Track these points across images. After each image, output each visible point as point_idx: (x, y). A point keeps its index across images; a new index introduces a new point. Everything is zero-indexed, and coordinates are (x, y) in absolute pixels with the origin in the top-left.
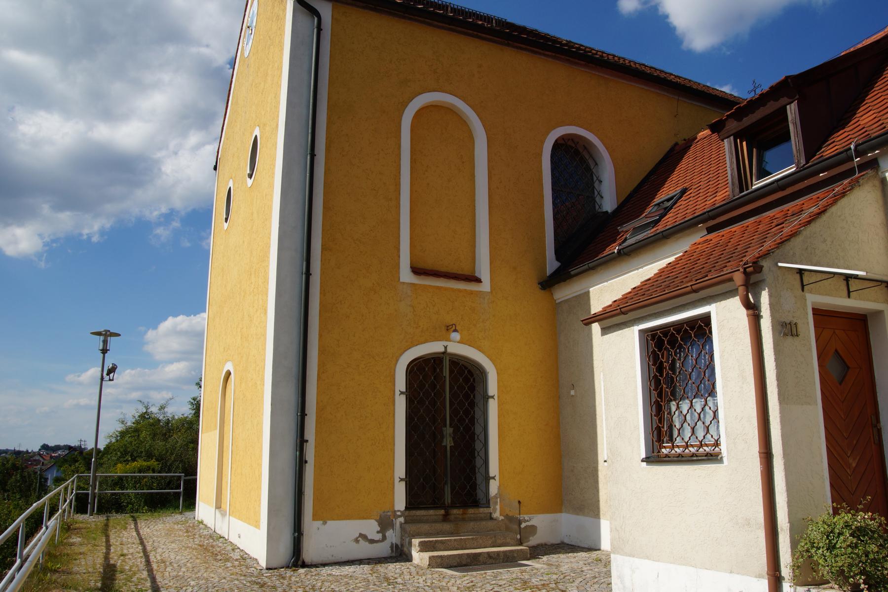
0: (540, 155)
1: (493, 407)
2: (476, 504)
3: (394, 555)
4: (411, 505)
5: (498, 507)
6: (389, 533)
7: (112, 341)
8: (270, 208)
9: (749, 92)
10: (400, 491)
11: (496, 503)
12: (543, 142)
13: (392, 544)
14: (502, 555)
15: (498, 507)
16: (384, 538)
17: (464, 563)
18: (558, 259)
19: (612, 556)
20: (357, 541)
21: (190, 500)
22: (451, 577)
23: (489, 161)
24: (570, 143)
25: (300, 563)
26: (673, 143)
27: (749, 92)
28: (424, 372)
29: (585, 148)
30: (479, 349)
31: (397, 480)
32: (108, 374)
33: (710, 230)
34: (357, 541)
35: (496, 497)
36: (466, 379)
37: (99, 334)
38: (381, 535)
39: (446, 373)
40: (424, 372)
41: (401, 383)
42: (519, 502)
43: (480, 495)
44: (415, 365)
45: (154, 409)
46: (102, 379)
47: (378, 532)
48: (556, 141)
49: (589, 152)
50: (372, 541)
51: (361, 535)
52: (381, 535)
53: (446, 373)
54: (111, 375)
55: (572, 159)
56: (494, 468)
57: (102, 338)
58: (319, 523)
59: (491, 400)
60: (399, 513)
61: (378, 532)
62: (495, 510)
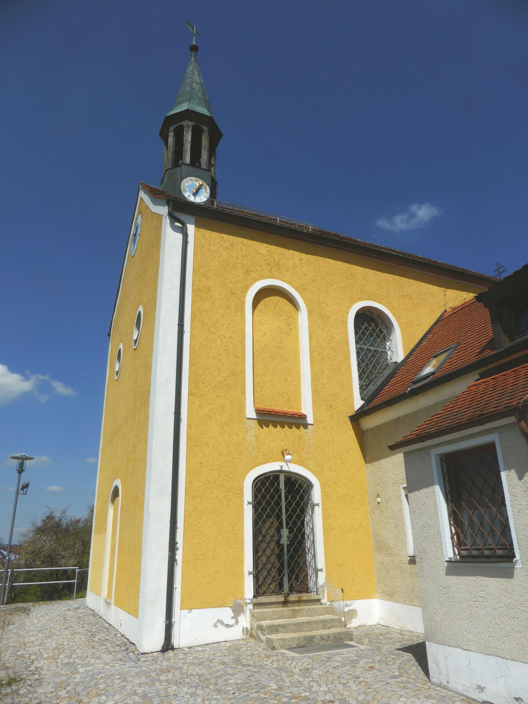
0: (345, 322)
1: (318, 512)
2: (307, 590)
3: (244, 637)
4: (257, 593)
5: (326, 594)
6: (241, 618)
7: (27, 463)
8: (242, 542)
9: (494, 271)
10: (249, 583)
11: (323, 590)
12: (347, 313)
13: (244, 628)
14: (331, 636)
15: (326, 594)
16: (237, 622)
17: (302, 644)
18: (362, 399)
19: (427, 643)
20: (215, 626)
21: (82, 588)
22: (293, 659)
23: (310, 327)
24: (368, 313)
25: (170, 647)
26: (443, 310)
27: (494, 271)
28: (269, 490)
29: (379, 316)
30: (307, 467)
31: (246, 573)
32: (22, 489)
33: (482, 376)
34: (215, 626)
35: (323, 586)
36: (296, 490)
37: (17, 458)
38: (234, 620)
39: (282, 486)
40: (265, 485)
41: (248, 495)
42: (342, 589)
43: (311, 584)
44: (259, 481)
45: (57, 514)
46: (18, 494)
47: (232, 618)
48: (357, 312)
49: (381, 319)
50: (228, 626)
51: (219, 621)
52: (234, 620)
53: (282, 486)
54: (25, 490)
55: (371, 325)
56: (321, 563)
57: (19, 461)
58: (185, 612)
59: (316, 508)
60: (249, 601)
61: (232, 618)
62: (324, 596)
